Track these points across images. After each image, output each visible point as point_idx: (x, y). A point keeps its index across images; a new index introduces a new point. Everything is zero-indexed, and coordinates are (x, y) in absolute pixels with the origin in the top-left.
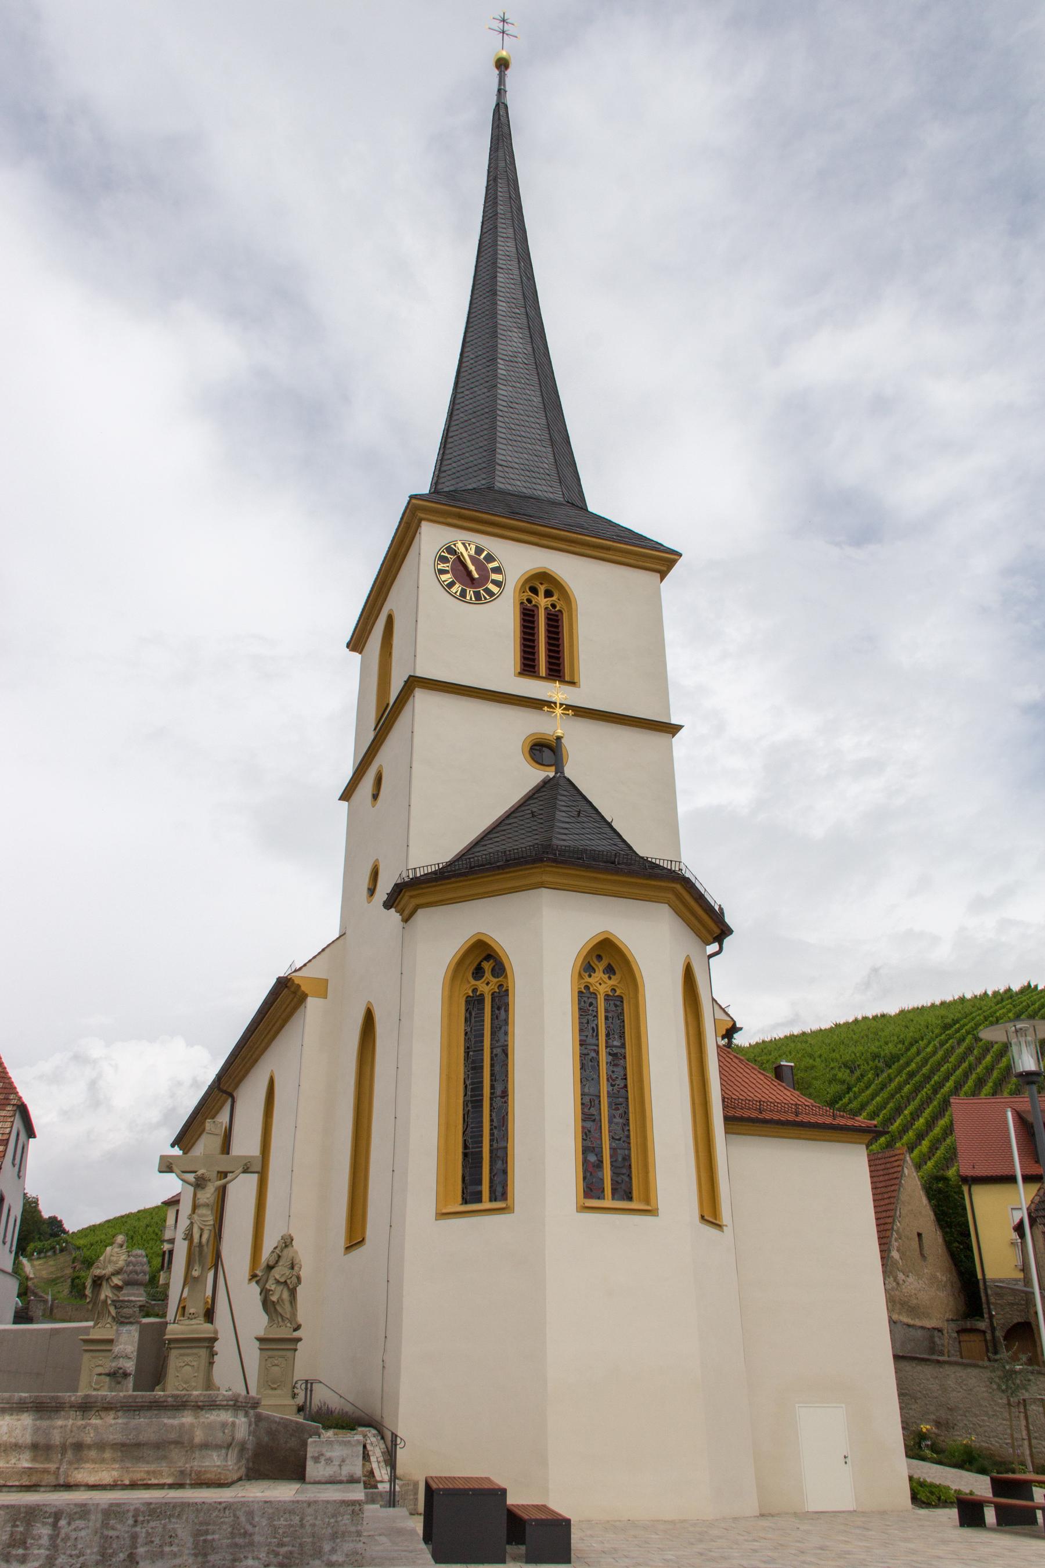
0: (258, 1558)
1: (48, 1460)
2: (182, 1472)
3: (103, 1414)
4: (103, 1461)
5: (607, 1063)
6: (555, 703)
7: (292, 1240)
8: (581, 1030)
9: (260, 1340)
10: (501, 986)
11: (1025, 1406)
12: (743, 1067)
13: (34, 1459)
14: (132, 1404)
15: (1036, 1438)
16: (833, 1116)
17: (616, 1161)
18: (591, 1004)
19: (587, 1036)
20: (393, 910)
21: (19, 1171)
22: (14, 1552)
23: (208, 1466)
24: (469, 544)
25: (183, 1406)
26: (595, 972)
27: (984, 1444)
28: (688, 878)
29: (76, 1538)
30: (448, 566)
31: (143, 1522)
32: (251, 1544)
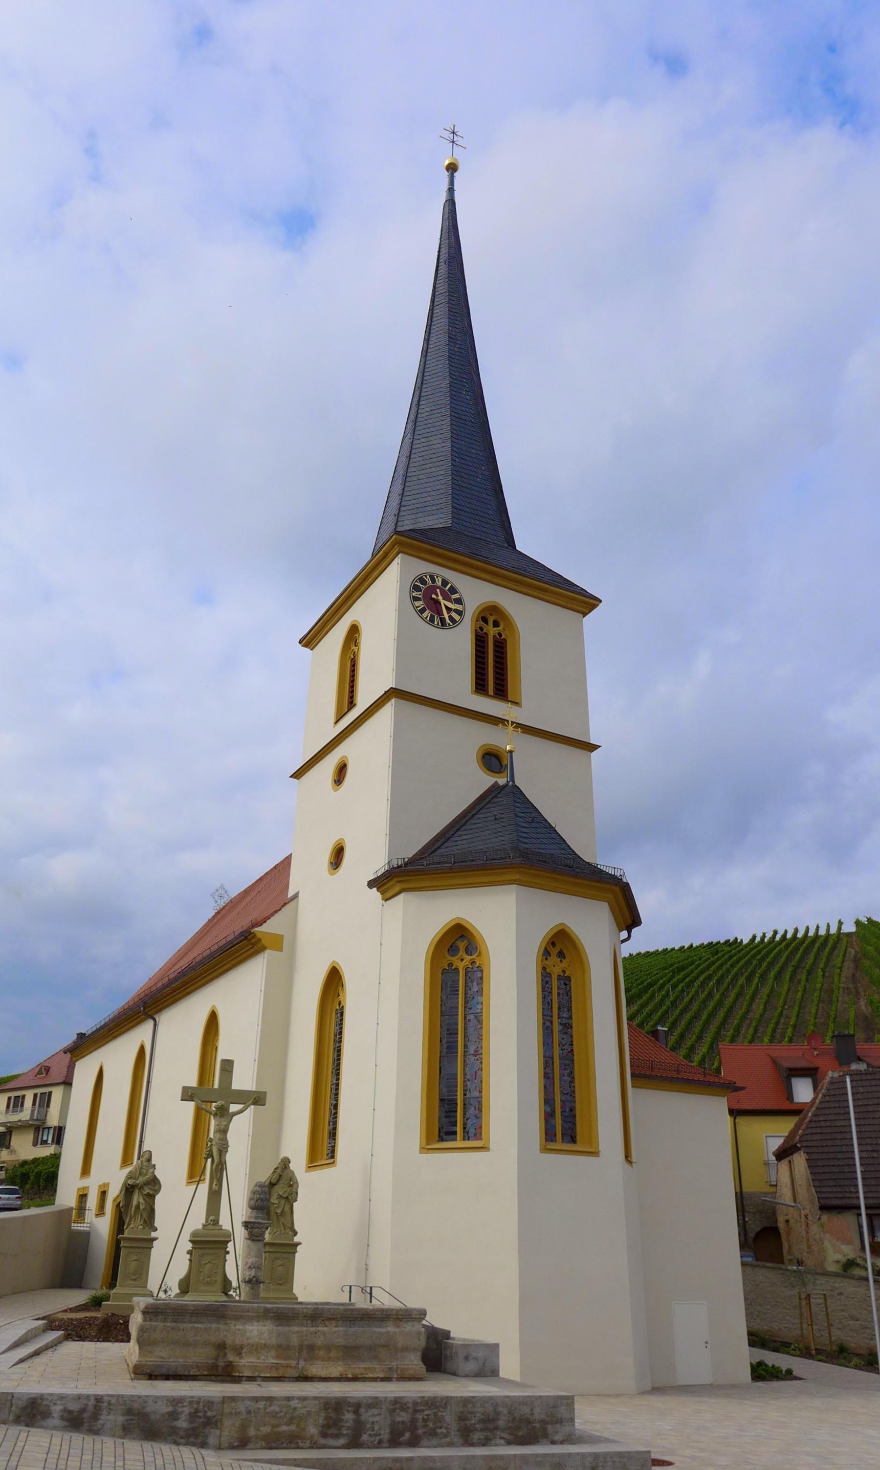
1: (289, 1358)
2: (390, 1369)
3: (327, 1323)
4: (329, 1359)
5: (559, 1031)
6: (508, 721)
7: (290, 1162)
10: (473, 963)
14: (350, 1316)
16: (704, 1074)
17: (564, 1111)
23: (408, 1365)
25: (386, 1318)
30: (420, 594)
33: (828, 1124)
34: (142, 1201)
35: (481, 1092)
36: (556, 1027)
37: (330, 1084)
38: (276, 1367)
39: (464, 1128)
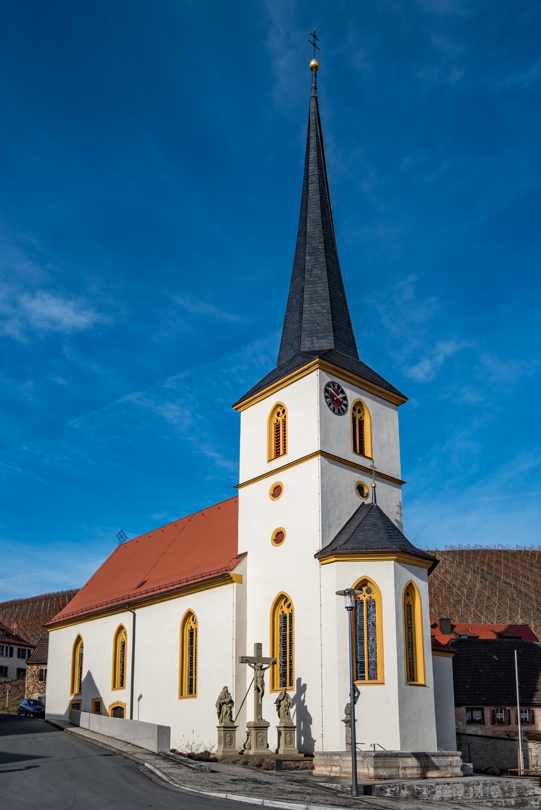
35: (376, 658)
37: (279, 651)
39: (369, 675)
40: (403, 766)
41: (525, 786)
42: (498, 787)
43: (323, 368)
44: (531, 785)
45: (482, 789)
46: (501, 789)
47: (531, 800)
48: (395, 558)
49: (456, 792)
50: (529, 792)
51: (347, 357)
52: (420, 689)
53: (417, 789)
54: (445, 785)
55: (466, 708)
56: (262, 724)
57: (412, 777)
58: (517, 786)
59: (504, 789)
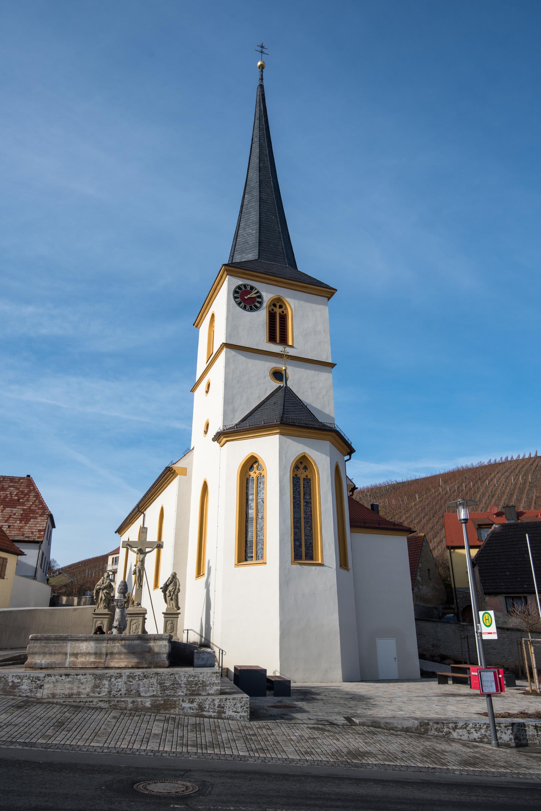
0: (183, 692)
4: (121, 659)
5: (304, 506)
7: (176, 575)
8: (294, 492)
9: (163, 613)
11: (467, 638)
12: (358, 505)
13: (95, 658)
15: (471, 651)
18: (298, 482)
19: (296, 495)
20: (216, 442)
21: (49, 542)
22: (96, 690)
24: (248, 286)
26: (299, 469)
27: (451, 654)
28: (338, 431)
29: (118, 685)
31: (142, 679)
32: (181, 687)
33: (492, 551)
34: (103, 596)
36: (302, 503)
38: (94, 663)
39: (256, 554)
40: (72, 652)
41: (203, 681)
42: (154, 681)
43: (233, 274)
44: (214, 679)
45: (125, 683)
46: (160, 684)
47: (183, 701)
48: (279, 431)
49: (78, 687)
50: (210, 689)
51: (271, 264)
52: (314, 569)
53: (13, 682)
54: (61, 676)
55: (505, 597)
56: (136, 611)
57: (84, 666)
58: (189, 680)
59: (164, 683)
